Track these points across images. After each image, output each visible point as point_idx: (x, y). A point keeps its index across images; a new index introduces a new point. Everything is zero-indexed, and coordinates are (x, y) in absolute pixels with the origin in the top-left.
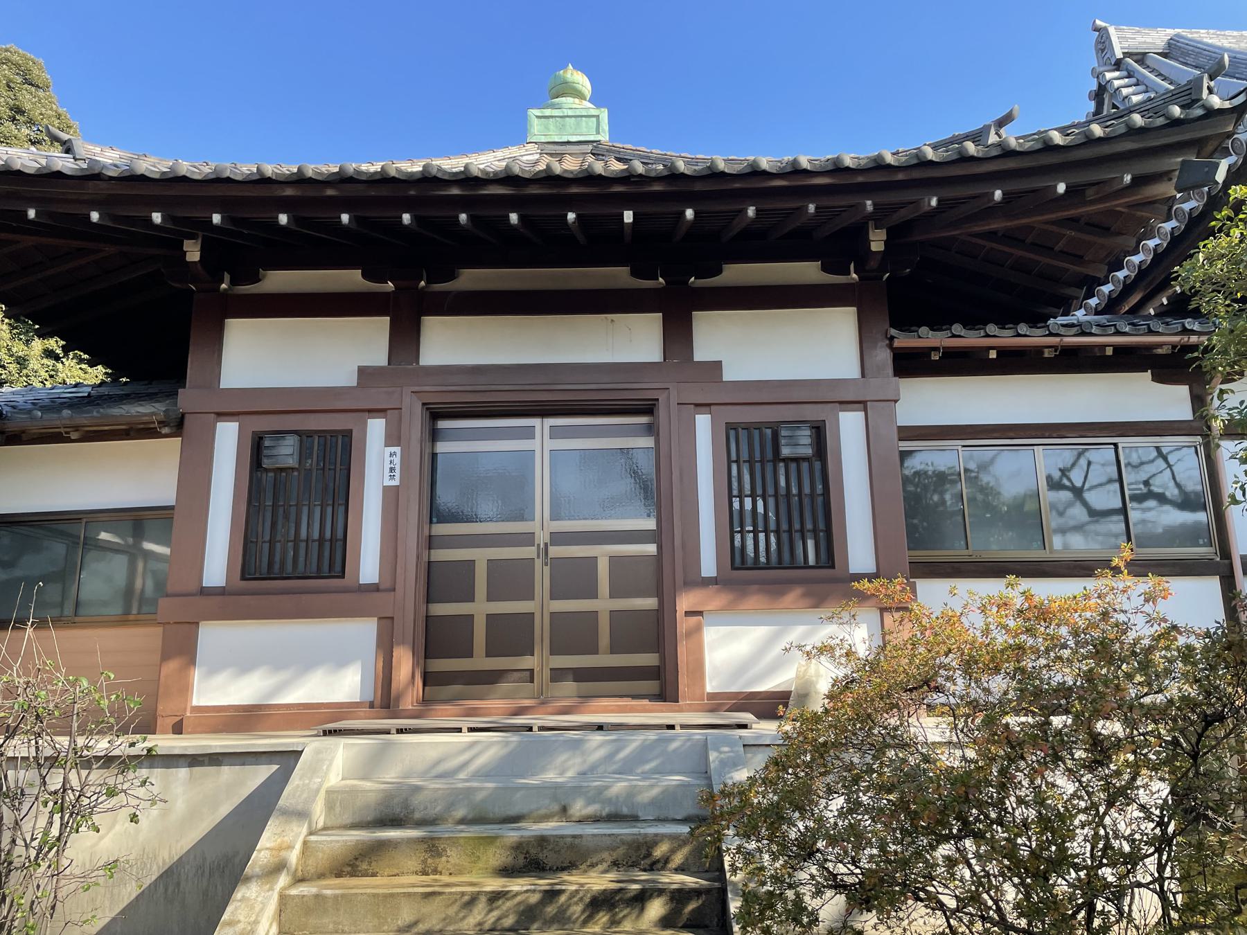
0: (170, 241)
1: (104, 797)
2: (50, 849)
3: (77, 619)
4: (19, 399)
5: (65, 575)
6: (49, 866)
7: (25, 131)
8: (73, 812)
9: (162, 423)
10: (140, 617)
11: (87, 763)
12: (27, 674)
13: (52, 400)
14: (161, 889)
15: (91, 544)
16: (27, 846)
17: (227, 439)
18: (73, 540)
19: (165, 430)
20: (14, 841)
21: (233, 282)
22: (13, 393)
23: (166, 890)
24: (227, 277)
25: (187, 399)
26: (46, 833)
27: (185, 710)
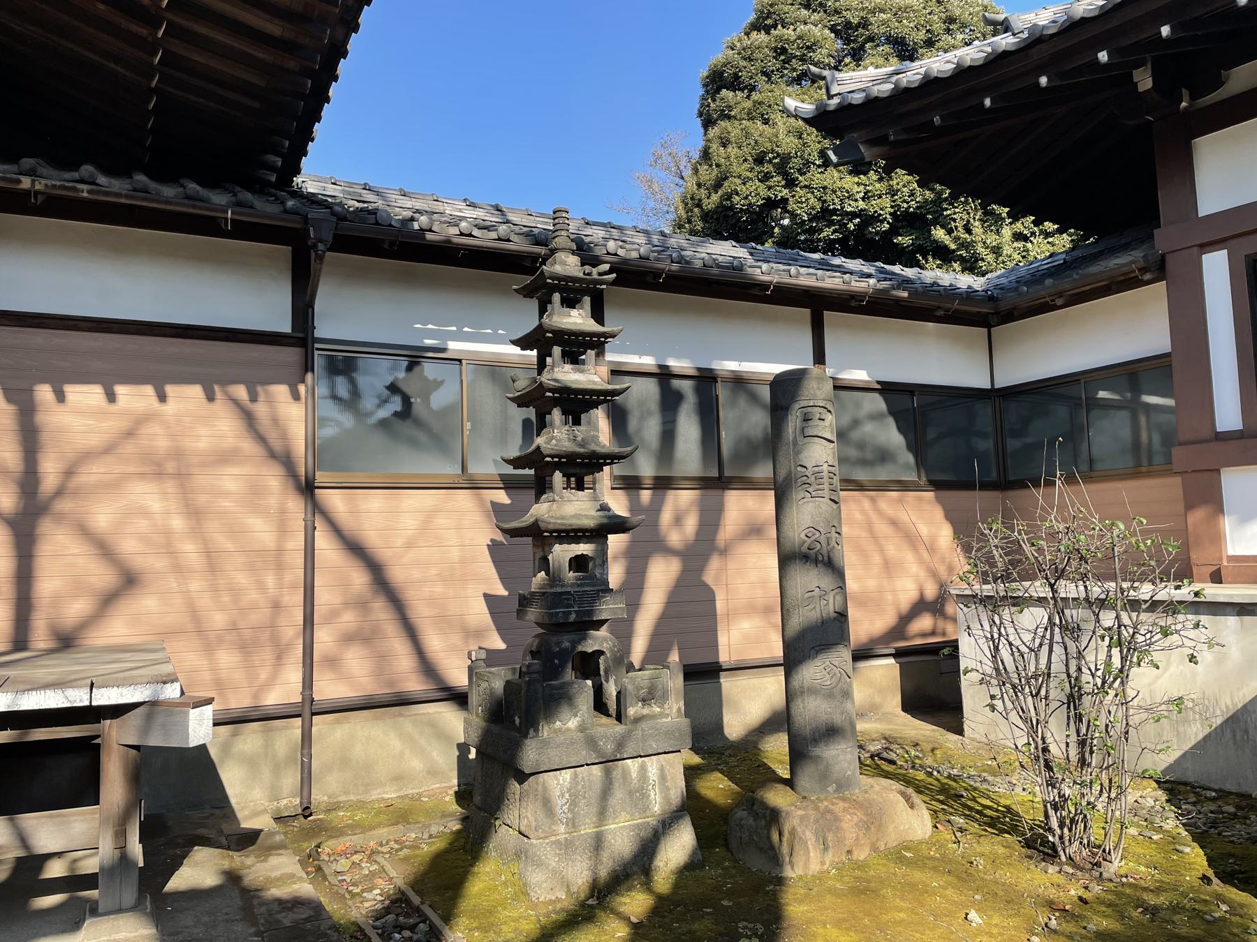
0: (1119, 75)
1: (1159, 636)
2: (1115, 679)
3: (1093, 474)
4: (1003, 281)
5: (1075, 435)
6: (1116, 695)
7: (960, 37)
8: (1130, 649)
9: (1143, 270)
10: (1152, 468)
11: (1134, 605)
12: (1065, 521)
13: (1033, 275)
14: (1228, 735)
15: (1094, 404)
16: (1093, 675)
17: (1217, 270)
18: (1075, 403)
19: (1148, 276)
20: (1079, 669)
21: (1193, 98)
22: (998, 277)
23: (1234, 736)
24: (1185, 92)
25: (1164, 239)
26: (1108, 663)
27: (1221, 559)
